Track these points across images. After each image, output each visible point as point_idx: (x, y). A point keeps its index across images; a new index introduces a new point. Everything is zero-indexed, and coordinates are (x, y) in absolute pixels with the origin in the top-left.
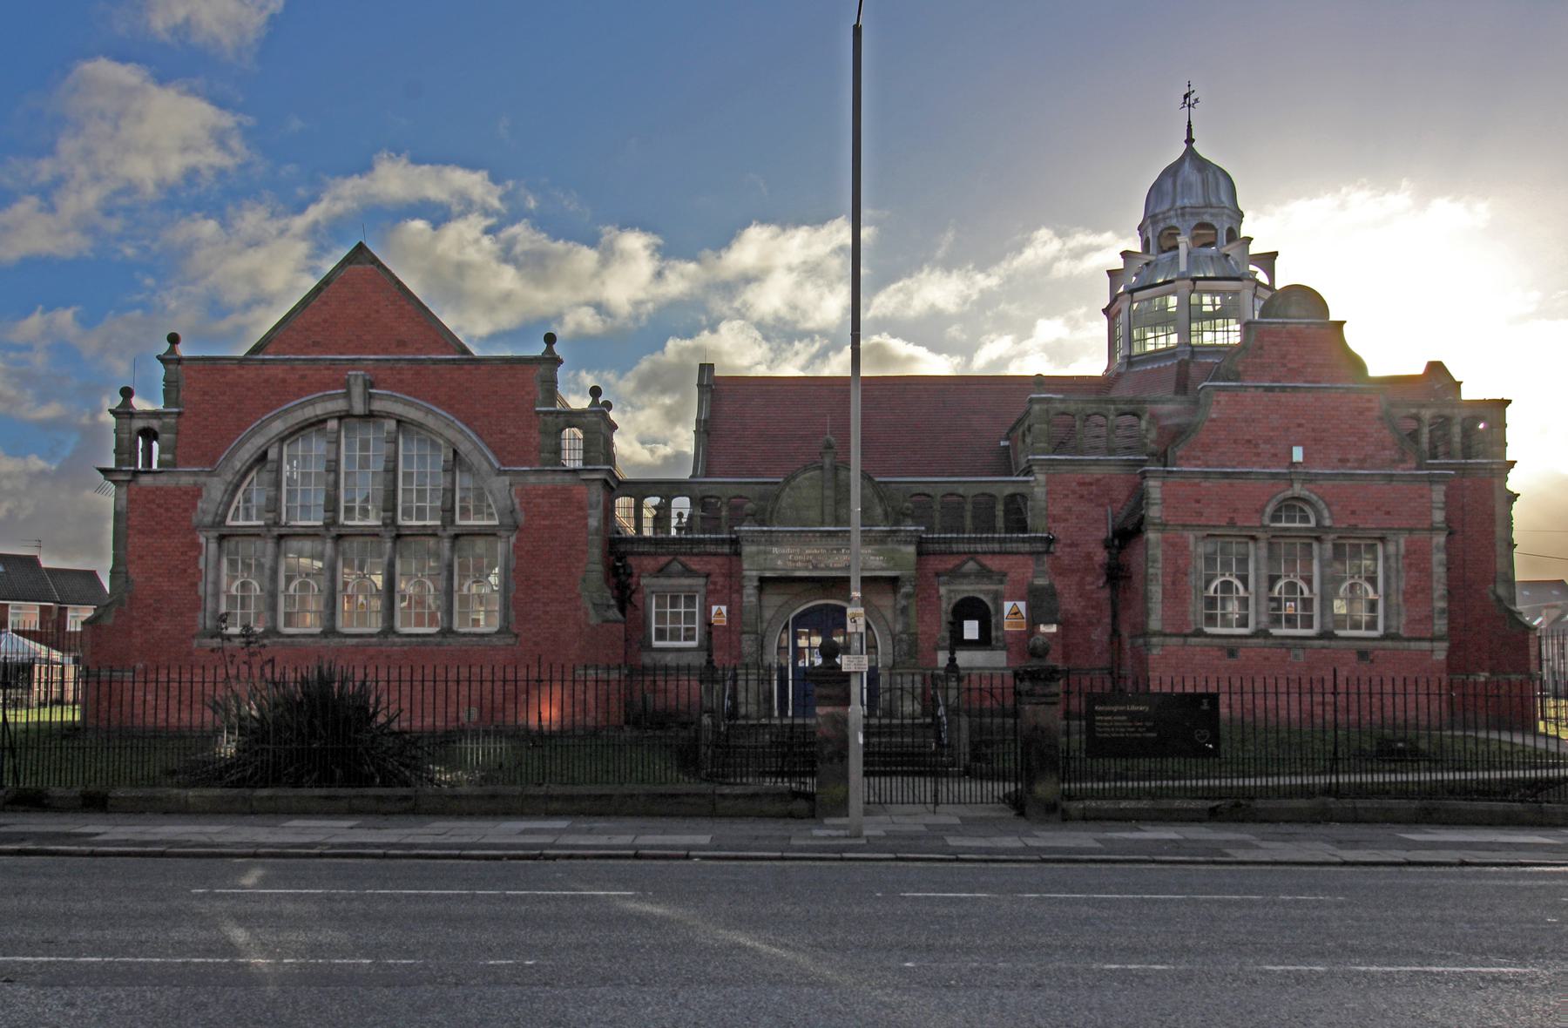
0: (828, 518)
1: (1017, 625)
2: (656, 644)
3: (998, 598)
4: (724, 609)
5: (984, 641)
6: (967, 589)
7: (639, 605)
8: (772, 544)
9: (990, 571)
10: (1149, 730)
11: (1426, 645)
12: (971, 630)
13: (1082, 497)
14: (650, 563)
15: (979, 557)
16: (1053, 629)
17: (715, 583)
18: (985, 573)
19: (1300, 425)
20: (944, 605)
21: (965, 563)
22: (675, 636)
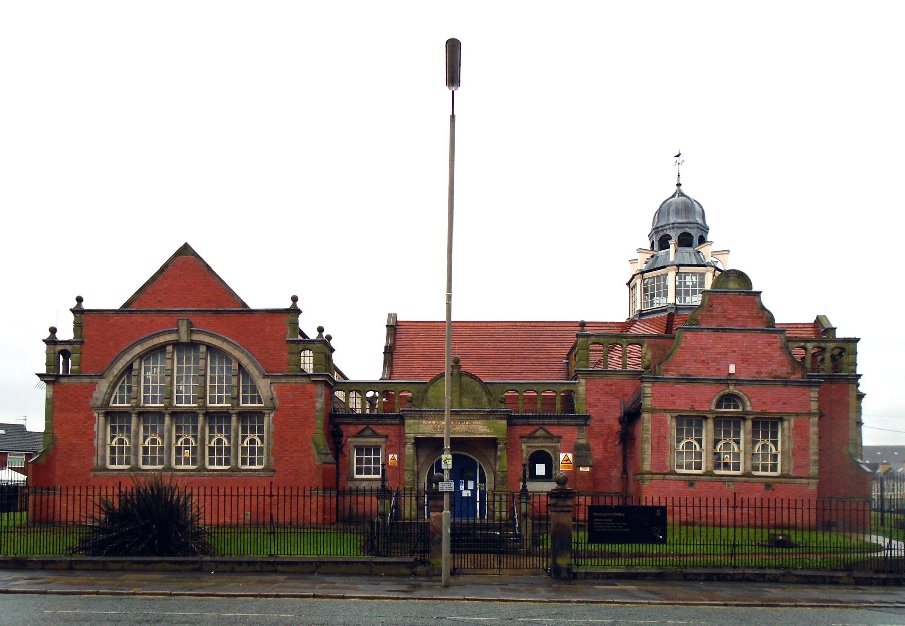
0: (455, 404)
1: (569, 467)
2: (357, 476)
3: (557, 452)
4: (396, 456)
5: (548, 477)
6: (538, 445)
7: (347, 453)
8: (422, 418)
9: (551, 435)
10: (625, 527)
11: (805, 481)
12: (540, 469)
13: (606, 392)
14: (352, 430)
15: (546, 428)
16: (588, 469)
17: (391, 441)
18: (550, 437)
19: (734, 352)
20: (524, 455)
21: (538, 430)
22: (368, 471)
